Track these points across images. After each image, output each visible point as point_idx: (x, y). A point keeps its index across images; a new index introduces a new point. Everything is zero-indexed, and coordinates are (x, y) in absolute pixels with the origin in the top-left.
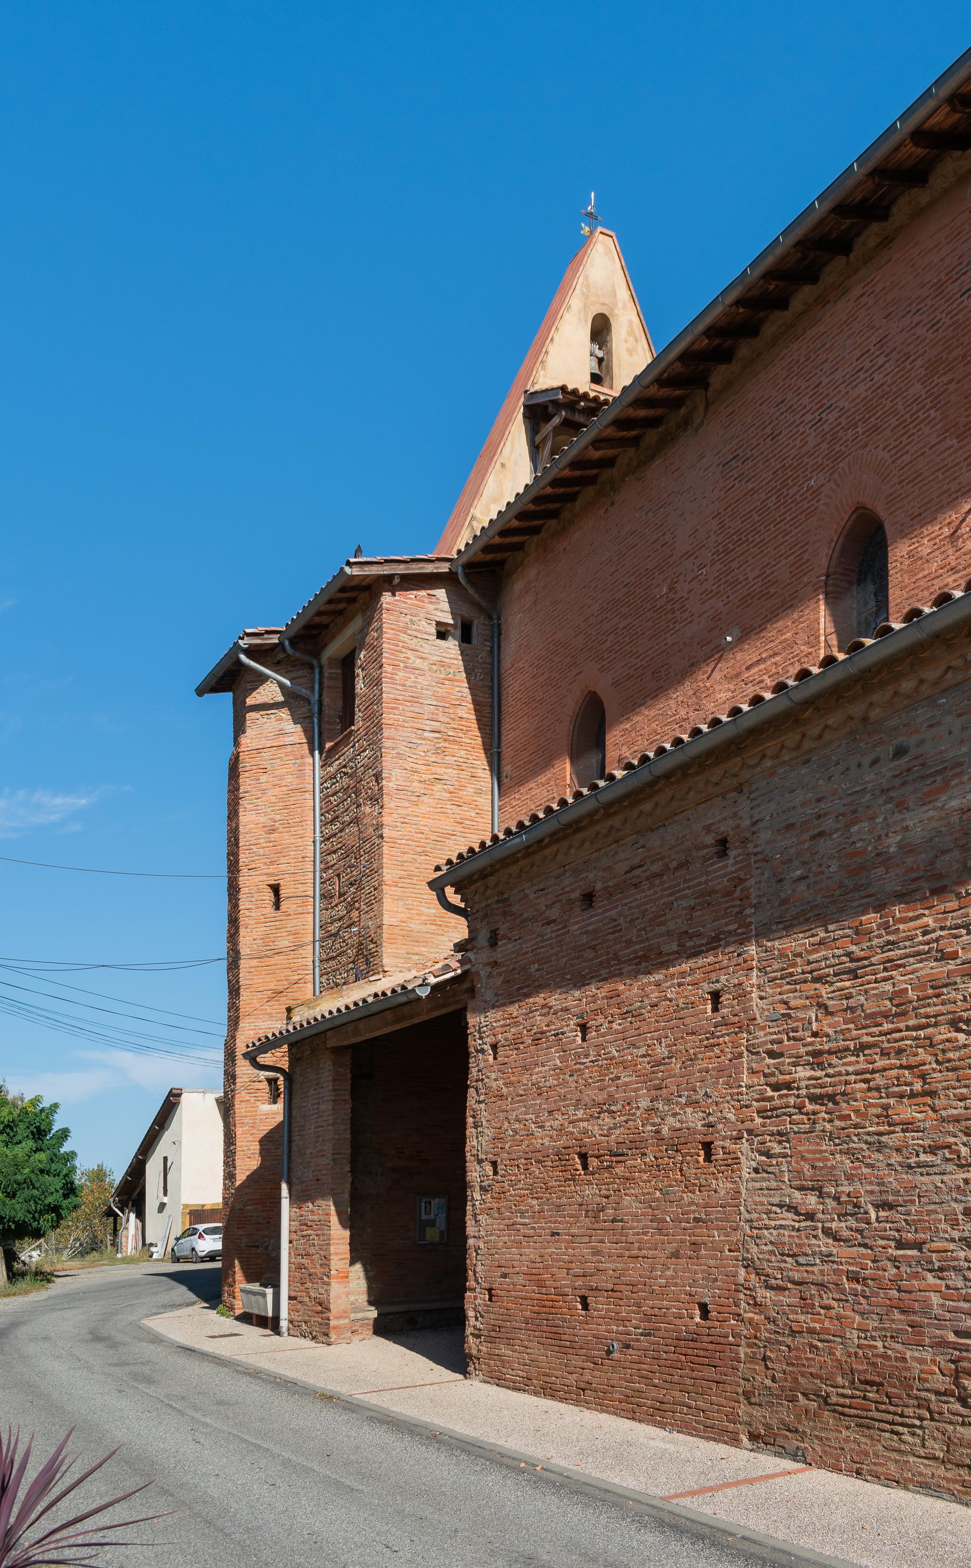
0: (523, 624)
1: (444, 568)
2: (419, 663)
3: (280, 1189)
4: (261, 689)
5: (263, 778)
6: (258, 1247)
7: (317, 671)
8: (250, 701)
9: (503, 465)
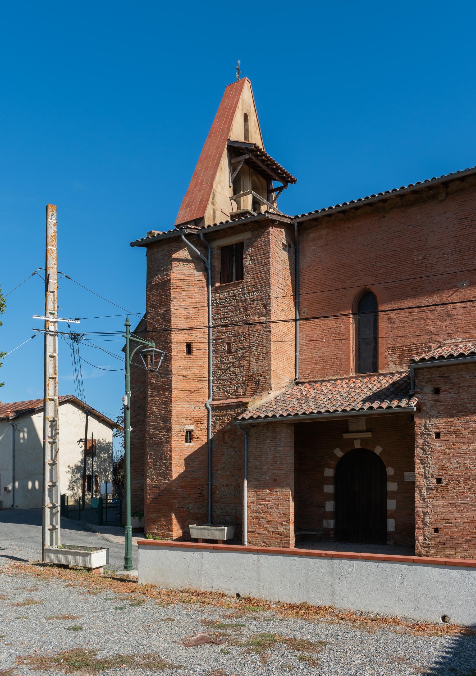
0: (311, 250)
1: (288, 221)
2: (278, 259)
3: (244, 482)
4: (180, 252)
5: (184, 293)
6: (184, 508)
7: (210, 250)
8: (174, 256)
9: (221, 168)
